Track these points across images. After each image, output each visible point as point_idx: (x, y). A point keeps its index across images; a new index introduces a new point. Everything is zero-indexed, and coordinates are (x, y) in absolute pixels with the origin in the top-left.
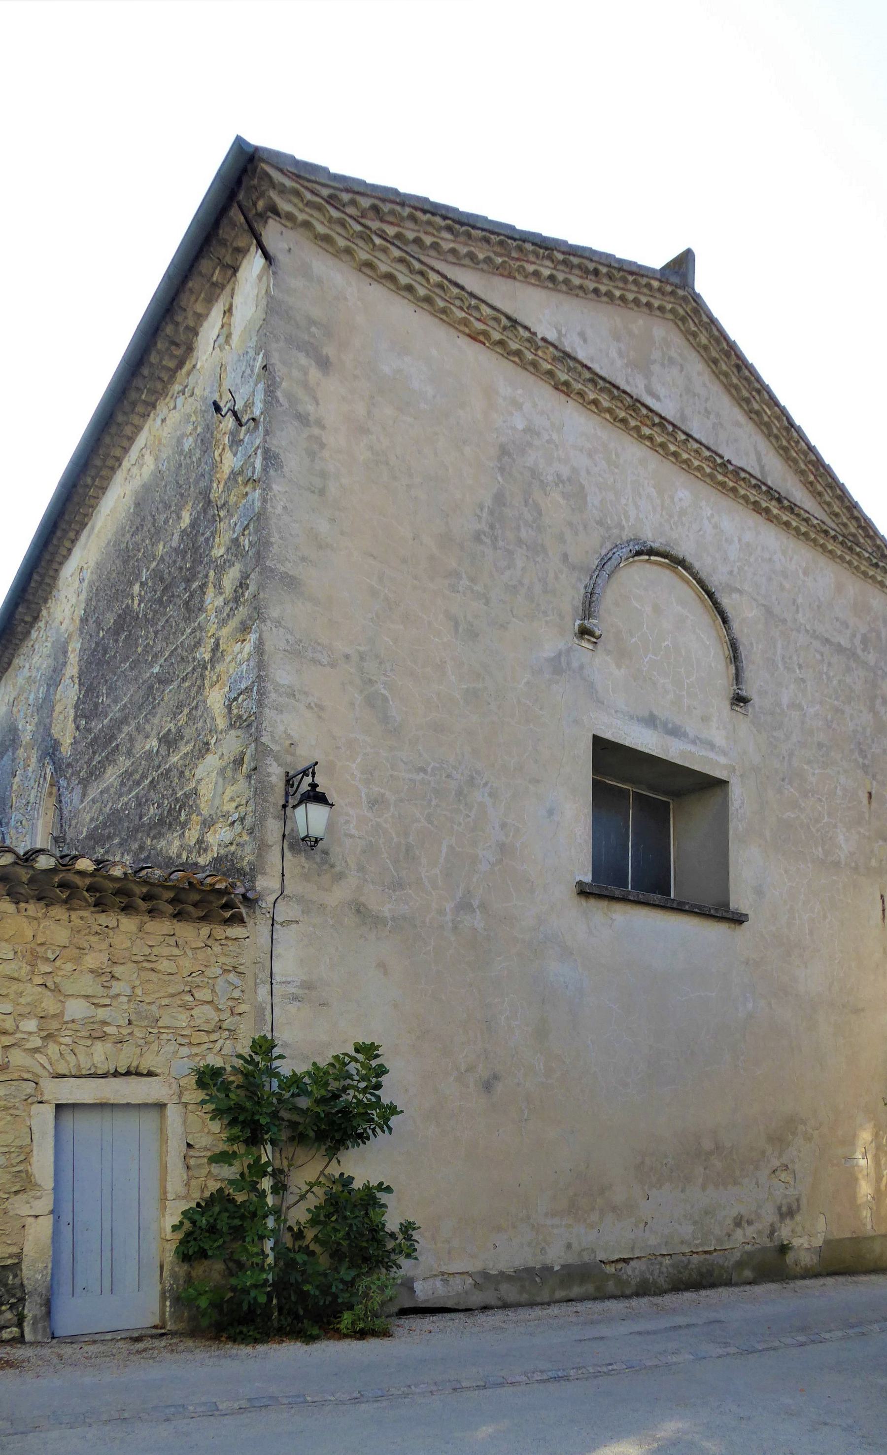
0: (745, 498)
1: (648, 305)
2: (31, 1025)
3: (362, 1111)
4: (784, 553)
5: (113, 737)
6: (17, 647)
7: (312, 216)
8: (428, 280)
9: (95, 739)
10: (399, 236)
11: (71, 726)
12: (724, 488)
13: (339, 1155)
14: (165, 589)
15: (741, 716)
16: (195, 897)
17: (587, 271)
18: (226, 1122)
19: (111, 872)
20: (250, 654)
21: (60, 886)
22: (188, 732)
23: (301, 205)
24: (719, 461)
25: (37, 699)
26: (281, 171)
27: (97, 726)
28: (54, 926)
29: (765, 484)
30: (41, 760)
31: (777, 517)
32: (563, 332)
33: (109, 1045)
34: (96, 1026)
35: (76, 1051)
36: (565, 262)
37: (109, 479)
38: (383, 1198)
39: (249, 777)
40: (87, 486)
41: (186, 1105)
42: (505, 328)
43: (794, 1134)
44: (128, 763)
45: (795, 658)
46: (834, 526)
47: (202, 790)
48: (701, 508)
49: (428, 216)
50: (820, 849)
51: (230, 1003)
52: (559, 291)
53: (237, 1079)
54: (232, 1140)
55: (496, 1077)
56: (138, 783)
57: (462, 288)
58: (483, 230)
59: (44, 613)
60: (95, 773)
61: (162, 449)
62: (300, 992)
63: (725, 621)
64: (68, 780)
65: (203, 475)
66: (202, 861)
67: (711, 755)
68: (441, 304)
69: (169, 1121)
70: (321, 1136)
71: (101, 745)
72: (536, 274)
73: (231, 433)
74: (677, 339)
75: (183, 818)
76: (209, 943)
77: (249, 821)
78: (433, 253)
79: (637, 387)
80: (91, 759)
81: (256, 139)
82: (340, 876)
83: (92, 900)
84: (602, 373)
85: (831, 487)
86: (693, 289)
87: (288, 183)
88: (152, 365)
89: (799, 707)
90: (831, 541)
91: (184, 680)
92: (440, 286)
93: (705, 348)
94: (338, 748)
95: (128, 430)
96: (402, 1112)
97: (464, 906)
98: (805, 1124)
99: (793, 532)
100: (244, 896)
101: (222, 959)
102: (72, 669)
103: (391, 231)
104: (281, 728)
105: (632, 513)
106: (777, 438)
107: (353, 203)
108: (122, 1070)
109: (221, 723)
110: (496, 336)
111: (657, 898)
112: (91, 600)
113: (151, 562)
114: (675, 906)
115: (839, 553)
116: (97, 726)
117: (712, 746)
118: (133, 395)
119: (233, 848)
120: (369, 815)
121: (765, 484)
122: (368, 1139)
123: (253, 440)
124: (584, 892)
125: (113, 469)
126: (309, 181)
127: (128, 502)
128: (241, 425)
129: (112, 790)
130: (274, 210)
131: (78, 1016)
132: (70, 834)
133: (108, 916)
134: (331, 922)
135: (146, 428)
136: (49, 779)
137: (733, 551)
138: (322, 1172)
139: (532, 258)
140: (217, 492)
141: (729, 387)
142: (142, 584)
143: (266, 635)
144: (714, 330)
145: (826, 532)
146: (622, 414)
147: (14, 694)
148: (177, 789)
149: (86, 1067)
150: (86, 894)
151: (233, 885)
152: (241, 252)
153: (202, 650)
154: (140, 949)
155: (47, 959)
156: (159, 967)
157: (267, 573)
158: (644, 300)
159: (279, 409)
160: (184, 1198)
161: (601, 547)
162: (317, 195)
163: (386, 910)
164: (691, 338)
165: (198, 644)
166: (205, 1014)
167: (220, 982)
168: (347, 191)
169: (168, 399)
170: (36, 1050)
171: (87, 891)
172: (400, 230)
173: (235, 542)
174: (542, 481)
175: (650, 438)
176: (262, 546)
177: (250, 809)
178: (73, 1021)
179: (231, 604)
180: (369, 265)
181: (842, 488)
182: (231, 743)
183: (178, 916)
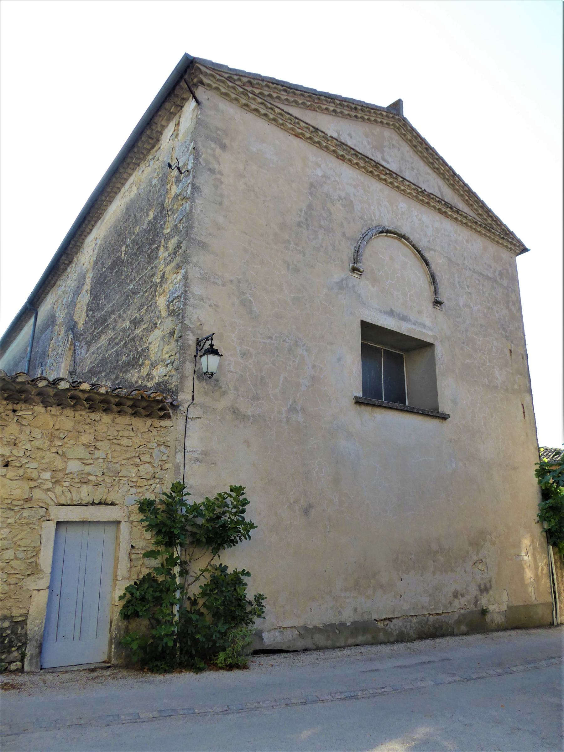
0: (434, 207)
1: (381, 122)
2: (47, 475)
3: (234, 526)
4: (456, 232)
5: (106, 320)
6: (60, 276)
7: (219, 85)
8: (274, 112)
11: (84, 315)
15: (439, 311)
16: (144, 404)
18: (154, 532)
19: (99, 391)
20: (181, 280)
22: (146, 318)
23: (214, 81)
24: (420, 190)
25: (67, 301)
27: (98, 315)
30: (66, 332)
32: (341, 133)
34: (84, 476)
35: (72, 490)
36: (340, 104)
37: (114, 198)
38: (245, 579)
39: (177, 341)
41: (132, 522)
42: (312, 132)
44: (113, 334)
45: (465, 282)
46: (480, 220)
47: (152, 348)
49: (275, 85)
50: (486, 379)
51: (161, 463)
52: (338, 116)
53: (162, 507)
54: (157, 543)
55: (311, 506)
56: (118, 344)
57: (291, 115)
58: (301, 91)
59: (75, 259)
60: (95, 339)
61: (141, 184)
63: (427, 264)
64: (80, 342)
65: (161, 196)
66: (149, 385)
67: (424, 330)
68: (281, 122)
69: (122, 532)
70: (209, 541)
71: (99, 324)
76: (151, 429)
77: (176, 364)
78: (277, 100)
80: (93, 332)
81: (194, 54)
82: (225, 393)
83: (87, 406)
85: (477, 202)
88: (139, 147)
89: (469, 306)
91: (145, 292)
92: (281, 114)
93: (410, 141)
95: (125, 176)
96: (257, 527)
97: (293, 409)
100: (171, 404)
101: (157, 438)
102: (87, 287)
104: (195, 316)
105: (377, 214)
106: (448, 180)
108: (97, 501)
109: (164, 314)
110: (308, 135)
111: (398, 405)
113: (132, 235)
114: (409, 410)
116: (98, 315)
117: (424, 326)
118: (129, 160)
119: (166, 378)
120: (241, 361)
124: (358, 402)
125: (116, 193)
127: (123, 208)
129: (103, 348)
130: (202, 83)
131: (74, 470)
132: (79, 370)
137: (430, 232)
138: (209, 563)
139: (325, 103)
140: (167, 203)
141: (423, 158)
142: (127, 246)
145: (476, 223)
146: (370, 169)
148: (138, 347)
151: (166, 398)
153: (156, 277)
154: (112, 432)
155: (60, 438)
157: (191, 241)
158: (379, 120)
159: (201, 166)
160: (127, 579)
161: (362, 229)
163: (249, 412)
164: (403, 136)
165: (154, 275)
166: (146, 469)
167: (156, 451)
168: (237, 75)
170: (49, 490)
171: (85, 401)
173: (176, 226)
174: (331, 199)
175: (385, 180)
176: (189, 229)
177: (177, 357)
178: (71, 473)
180: (246, 105)
182: (169, 324)
183: (135, 414)
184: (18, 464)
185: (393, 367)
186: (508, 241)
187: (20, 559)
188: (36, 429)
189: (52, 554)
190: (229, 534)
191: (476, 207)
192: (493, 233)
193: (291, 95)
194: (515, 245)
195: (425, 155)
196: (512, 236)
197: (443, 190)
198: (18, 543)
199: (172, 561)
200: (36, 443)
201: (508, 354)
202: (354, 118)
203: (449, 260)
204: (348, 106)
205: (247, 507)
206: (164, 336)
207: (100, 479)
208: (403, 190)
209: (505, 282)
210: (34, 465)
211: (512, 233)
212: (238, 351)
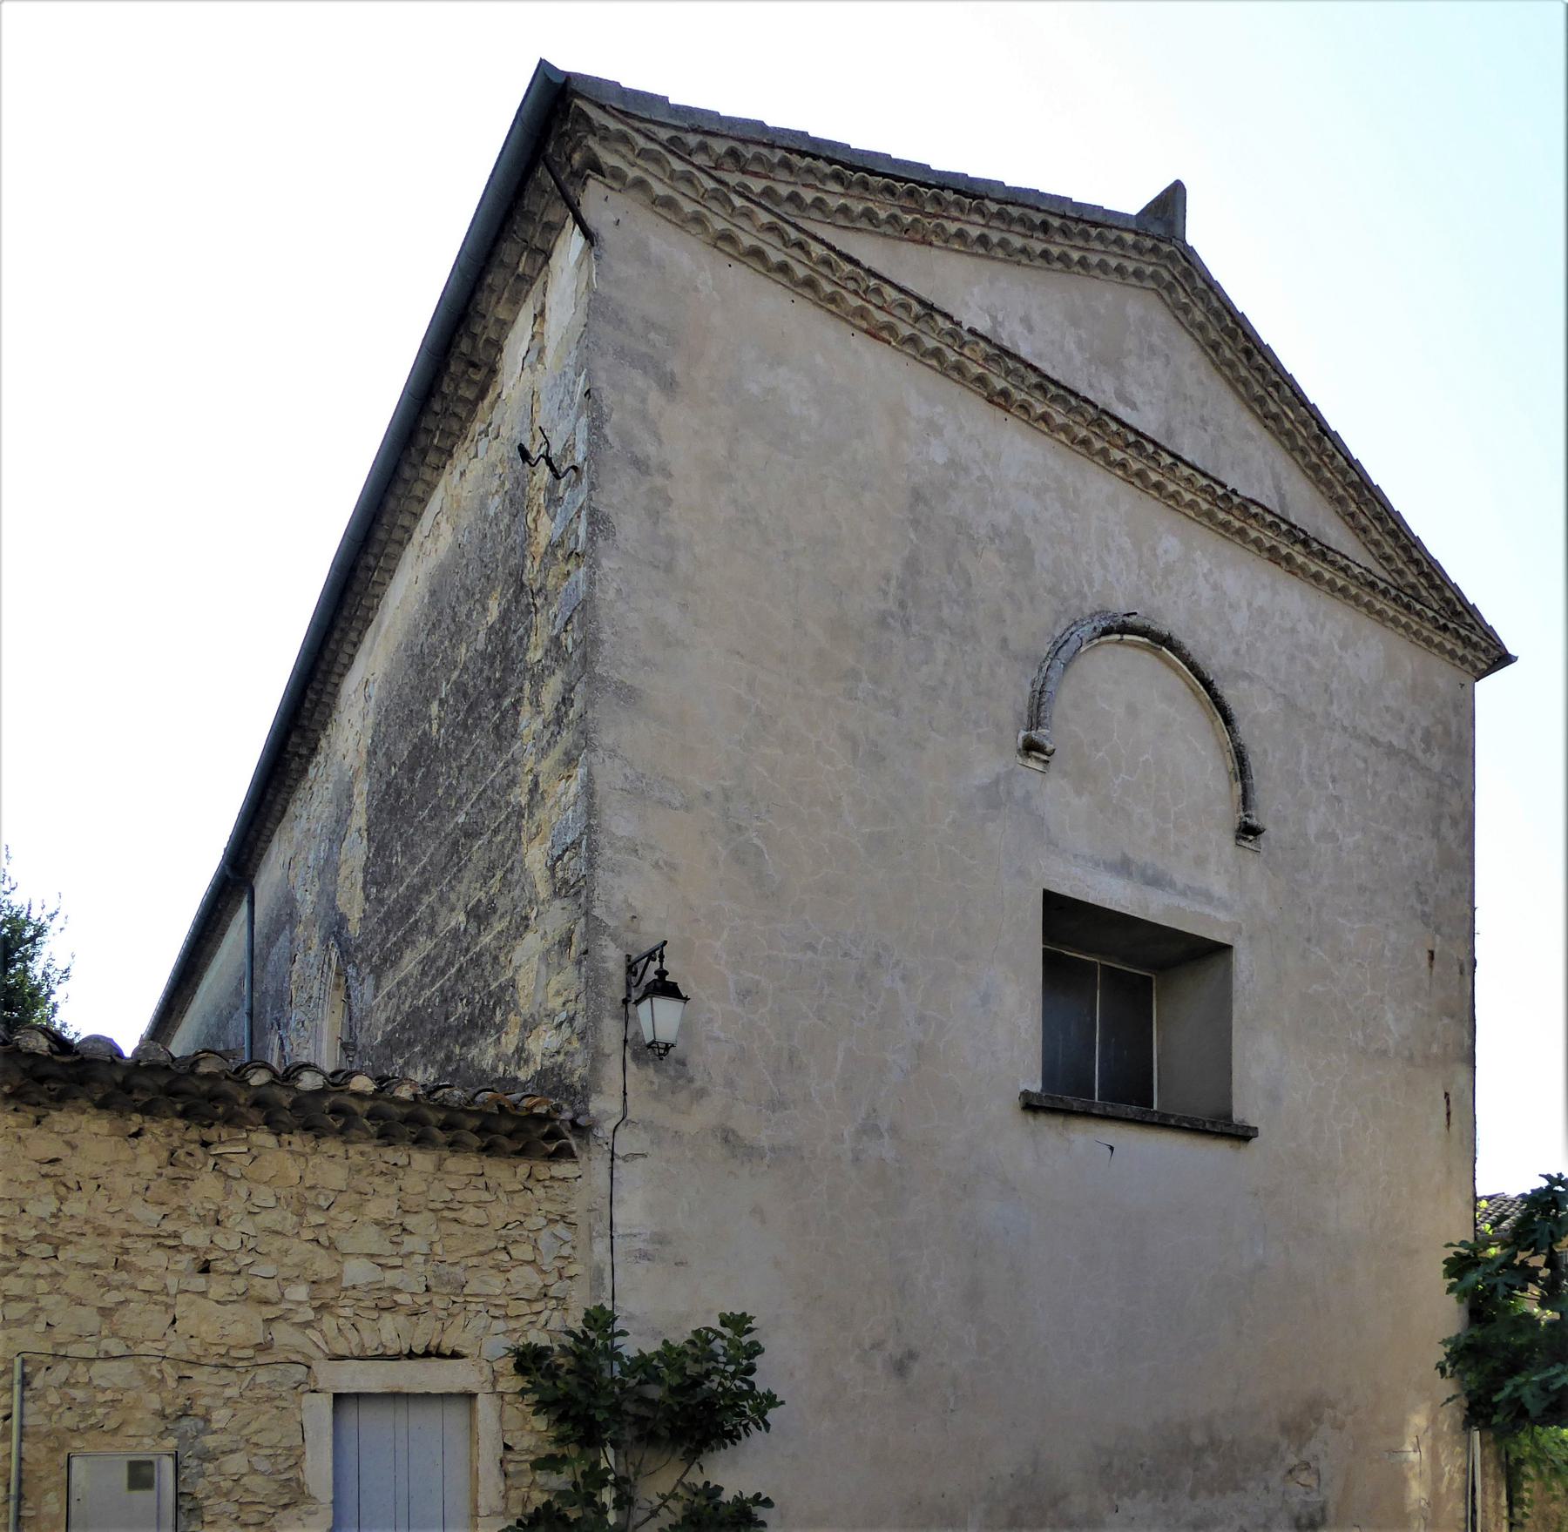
0: (1257, 542)
1: (1120, 269)
2: (300, 1292)
3: (729, 1402)
4: (1312, 619)
5: (411, 911)
6: (292, 790)
7: (646, 170)
8: (808, 254)
9: (389, 913)
10: (768, 192)
11: (360, 895)
12: (1227, 530)
13: (702, 1459)
14: (471, 709)
15: (1250, 854)
16: (509, 1125)
17: (1032, 227)
18: (553, 1418)
19: (396, 1094)
20: (576, 796)
21: (332, 1112)
22: (503, 903)
23: (631, 157)
24: (1220, 491)
25: (317, 858)
26: (602, 107)
27: (391, 895)
28: (326, 1165)
29: (1285, 521)
30: (324, 941)
31: (1302, 568)
32: (1000, 318)
33: (401, 1319)
34: (383, 1294)
35: (359, 1326)
36: (1000, 215)
37: (397, 558)
38: (761, 1513)
39: (579, 963)
40: (368, 568)
41: (502, 1395)
42: (917, 319)
43: (1318, 1420)
44: (430, 945)
45: (1327, 768)
46: (1384, 575)
47: (522, 981)
48: (1194, 561)
49: (808, 160)
50: (1359, 1034)
51: (559, 1263)
52: (994, 258)
53: (566, 1362)
54: (561, 1440)
55: (912, 1355)
56: (442, 972)
57: (856, 263)
58: (885, 175)
59: (323, 743)
60: (390, 959)
61: (463, 514)
62: (650, 1248)
63: (1228, 720)
64: (358, 968)
65: (513, 549)
66: (523, 1075)
67: (1207, 910)
68: (828, 288)
69: (481, 1416)
70: (677, 1436)
71: (398, 920)
72: (961, 235)
73: (548, 489)
74: (1160, 317)
75: (498, 1018)
76: (530, 1184)
77: (579, 1022)
78: (816, 215)
79: (1104, 392)
80: (385, 939)
81: (566, 63)
82: (701, 1093)
83: (374, 1130)
84: (1055, 376)
85: (1380, 520)
86: (1184, 241)
87: (613, 125)
88: (444, 396)
89: (1333, 837)
90: (1380, 597)
91: (496, 832)
92: (826, 262)
93: (1201, 328)
94: (697, 920)
95: (418, 489)
96: (782, 1403)
97: (869, 1129)
98: (1333, 1408)
99: (1325, 588)
100: (573, 1122)
101: (546, 1206)
102: (359, 820)
103: (757, 185)
104: (619, 897)
105: (1098, 574)
106: (1303, 452)
107: (703, 148)
108: (419, 1350)
109: (543, 891)
110: (905, 330)
111: (1132, 1110)
112: (379, 724)
113: (451, 671)
114: (1156, 1120)
115: (1391, 613)
116: (391, 895)
117: (1208, 897)
118: (422, 440)
119: (560, 1058)
120: (739, 1010)
121: (1285, 521)
122: (739, 1438)
123: (575, 497)
124: (1030, 1105)
125: (402, 544)
126: (643, 120)
127: (422, 588)
128: (557, 477)
129: (412, 981)
130: (595, 166)
131: (361, 1281)
132: (362, 1040)
133: (395, 1151)
134: (689, 1155)
135: (442, 483)
136: (334, 967)
137: (1240, 621)
138: (680, 1481)
139: (955, 213)
140: (531, 574)
141: (1235, 383)
142: (442, 702)
143: (597, 769)
144: (1213, 298)
145: (1372, 585)
146: (1083, 433)
147: (290, 853)
148: (490, 980)
149: (371, 1346)
150: (367, 1123)
151: (558, 1109)
152: (554, 229)
153: (517, 790)
154: (440, 1194)
155: (319, 1207)
156: (464, 1218)
157: (596, 683)
158: (1113, 262)
159: (611, 452)
160: (501, 1514)
161: (1055, 623)
162: (652, 140)
163: (764, 1139)
164: (1180, 314)
165: (513, 782)
166: (525, 1277)
167: (544, 1235)
168: (695, 130)
169: (467, 444)
170: (308, 1324)
171: (368, 1118)
172: (770, 183)
173: (556, 640)
174: (971, 537)
175: (1123, 465)
176: (590, 644)
177: (580, 1006)
178: (354, 1287)
179: (552, 728)
180: (727, 237)
181: (1397, 518)
182: (555, 918)
183: (489, 1150)
184: (230, 1268)
185: (1124, 1008)
186: (1458, 636)
187: (263, 1473)
188: (262, 1187)
189: (330, 1465)
190: (719, 1419)
191: (1377, 537)
192: (1418, 614)
193: (856, 191)
194: (1475, 646)
195: (1244, 373)
196: (1469, 620)
197: (1286, 486)
198: (254, 1439)
199: (596, 1478)
200: (266, 1219)
201: (1425, 962)
202: (1039, 262)
203: (1290, 704)
204: (1022, 220)
205: (758, 1360)
206: (548, 951)
207: (421, 1300)
208: (1173, 496)
209: (1436, 761)
210: (270, 1270)
211: (1472, 610)
212: (731, 984)
